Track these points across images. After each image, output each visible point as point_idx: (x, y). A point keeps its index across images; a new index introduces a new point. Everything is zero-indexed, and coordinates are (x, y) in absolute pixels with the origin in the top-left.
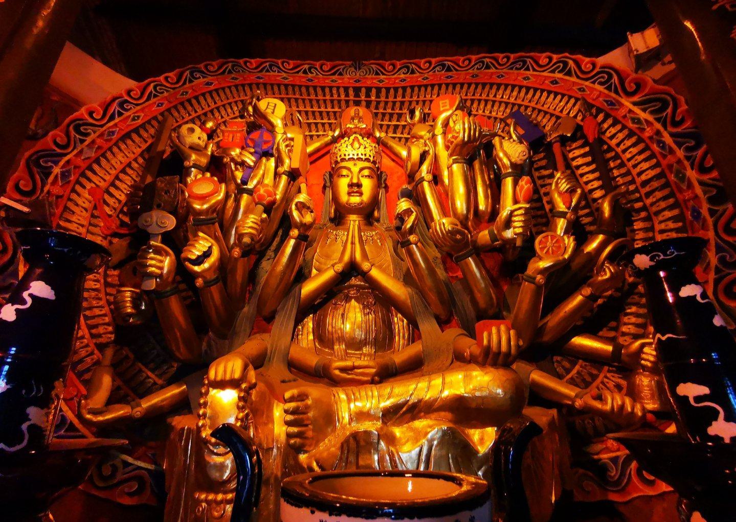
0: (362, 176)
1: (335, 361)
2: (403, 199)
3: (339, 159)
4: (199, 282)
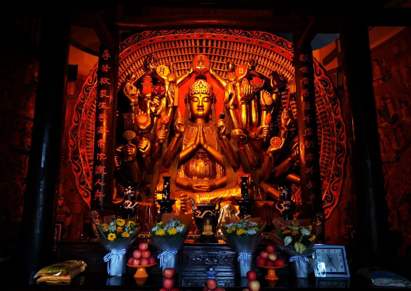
0: (204, 101)
1: (194, 184)
2: (221, 119)
3: (193, 93)
4: (144, 156)
